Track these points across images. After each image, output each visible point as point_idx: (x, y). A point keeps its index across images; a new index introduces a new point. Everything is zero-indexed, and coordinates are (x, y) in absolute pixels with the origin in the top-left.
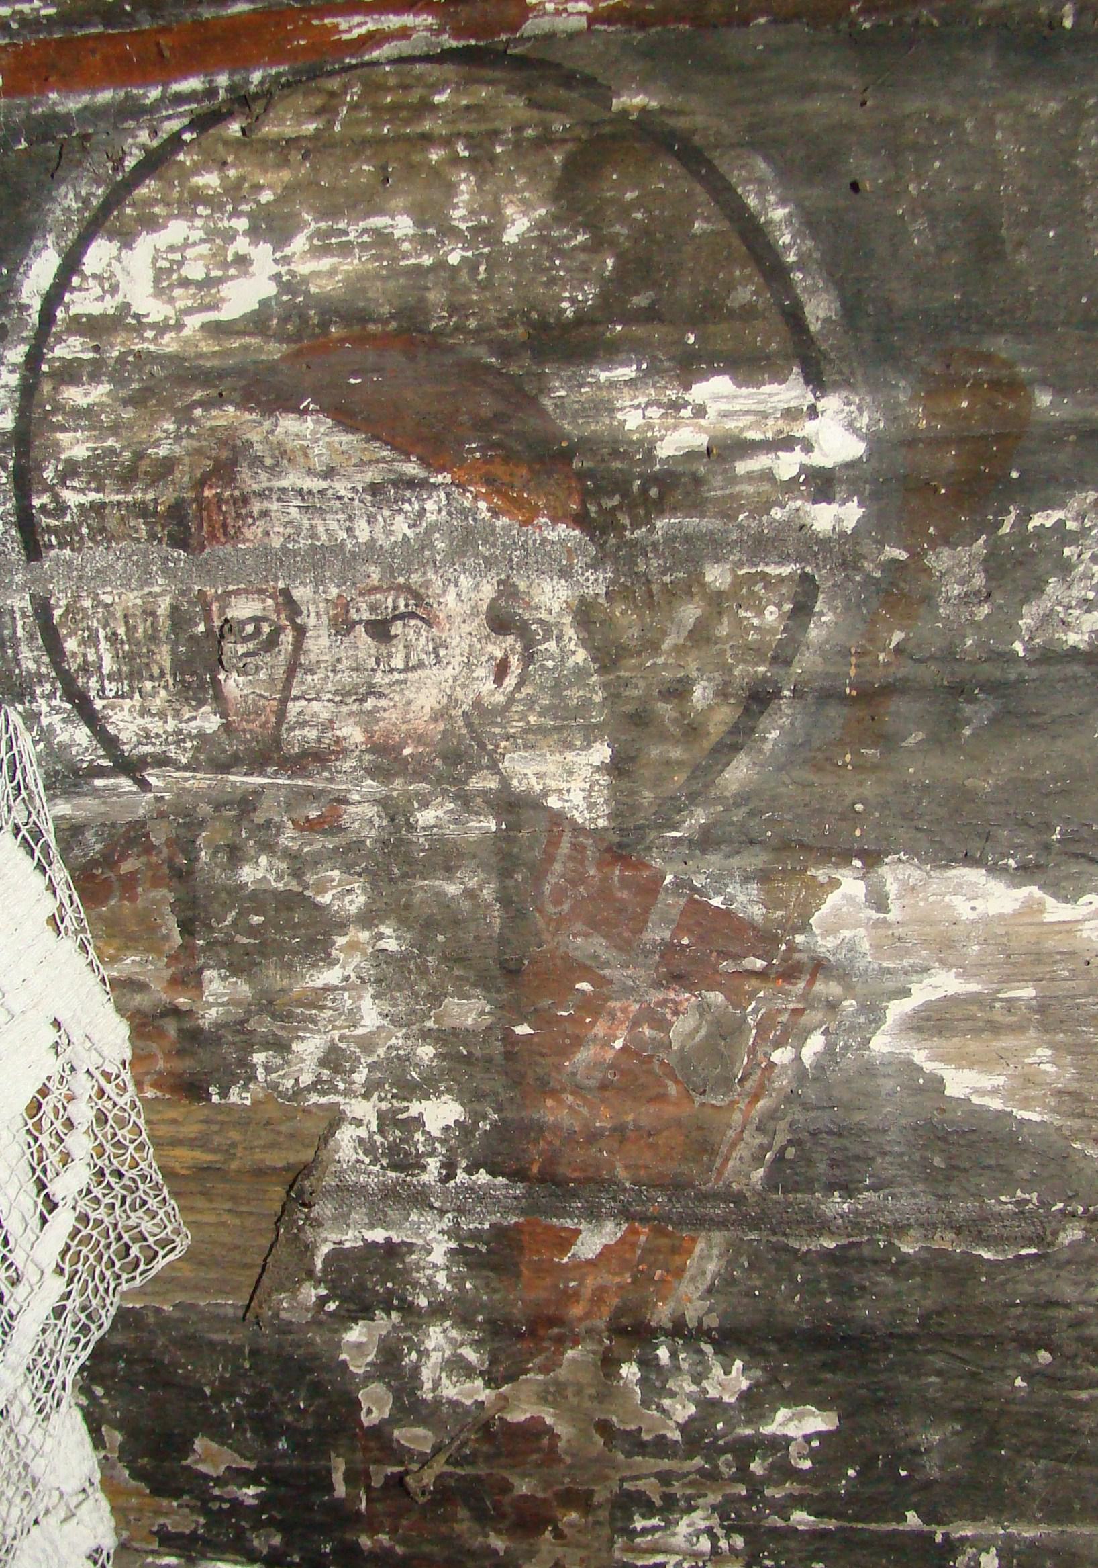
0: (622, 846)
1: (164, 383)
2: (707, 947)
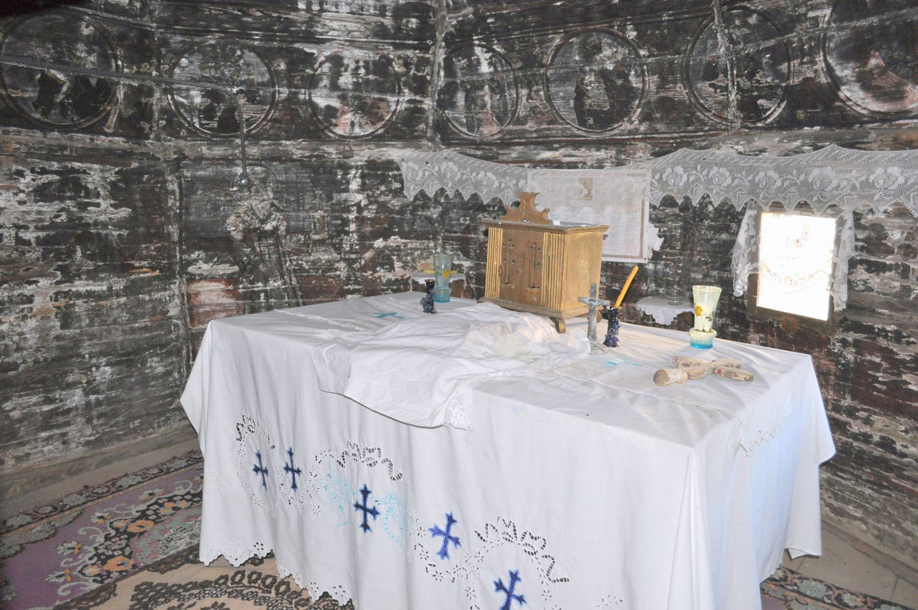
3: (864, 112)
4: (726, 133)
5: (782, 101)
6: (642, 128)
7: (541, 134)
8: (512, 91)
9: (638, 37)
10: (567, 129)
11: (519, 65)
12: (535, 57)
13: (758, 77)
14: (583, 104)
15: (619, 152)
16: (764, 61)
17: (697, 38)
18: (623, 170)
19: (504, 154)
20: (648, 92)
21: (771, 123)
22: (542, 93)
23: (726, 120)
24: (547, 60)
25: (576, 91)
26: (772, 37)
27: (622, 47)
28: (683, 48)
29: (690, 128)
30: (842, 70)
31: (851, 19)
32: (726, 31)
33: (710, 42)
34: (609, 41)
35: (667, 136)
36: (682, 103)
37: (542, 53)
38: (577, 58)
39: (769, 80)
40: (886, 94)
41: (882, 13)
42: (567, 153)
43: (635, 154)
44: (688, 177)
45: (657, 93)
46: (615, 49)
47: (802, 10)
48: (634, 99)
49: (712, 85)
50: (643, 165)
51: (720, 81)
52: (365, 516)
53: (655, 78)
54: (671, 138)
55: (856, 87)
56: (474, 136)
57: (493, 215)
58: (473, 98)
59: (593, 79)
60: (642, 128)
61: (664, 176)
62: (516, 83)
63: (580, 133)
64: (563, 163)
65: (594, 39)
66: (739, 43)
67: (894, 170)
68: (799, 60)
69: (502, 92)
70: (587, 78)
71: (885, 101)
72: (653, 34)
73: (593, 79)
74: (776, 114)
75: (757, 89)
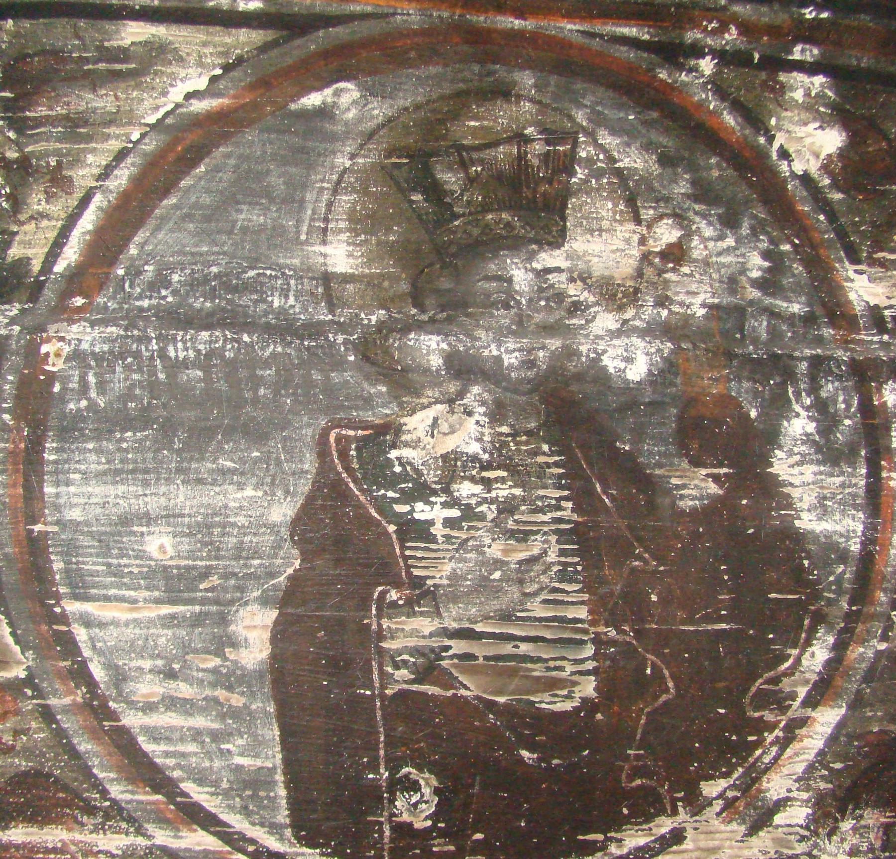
25: (303, 527)
27: (730, 222)
34: (634, 160)
38: (340, 256)
46: (667, 234)
48: (795, 625)
59: (469, 436)
65: (519, 113)
70: (417, 424)
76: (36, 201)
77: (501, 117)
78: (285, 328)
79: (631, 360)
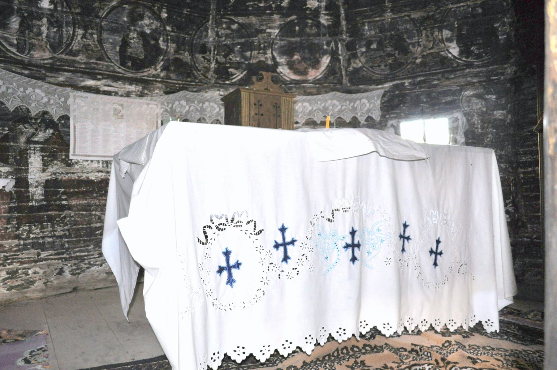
0: (487, 111)
1: (467, 97)
2: (490, 114)
3: (288, 79)
4: (206, 85)
5: (244, 70)
6: (162, 75)
7: (88, 66)
8: (69, 28)
9: (167, 17)
10: (112, 66)
11: (78, 11)
12: (94, 9)
13: (231, 57)
14: (126, 51)
15: (144, 88)
16: (236, 49)
17: (199, 29)
18: (144, 100)
19: (51, 77)
20: (169, 53)
21: (235, 82)
22: (95, 36)
23: (207, 78)
24: (102, 14)
25: (122, 40)
26: (243, 37)
27: (157, 21)
28: (190, 32)
29: (189, 79)
30: (280, 59)
31: (288, 36)
32: (216, 29)
33: (204, 33)
34: (150, 15)
35: (175, 82)
36: (186, 63)
37: (100, 8)
38: (125, 19)
39: (238, 59)
40: (299, 72)
41: (302, 36)
42: (107, 83)
43: (154, 90)
44: (190, 107)
45: (174, 54)
46: (152, 21)
47: (264, 28)
48: (160, 55)
49: (203, 57)
50: (155, 98)
51: (207, 55)
52: (404, 242)
53: (174, 45)
54: (178, 84)
55: (286, 68)
56: (24, 57)
57: (35, 127)
58: (29, 25)
59: (135, 36)
60: (162, 75)
61: (174, 106)
62: (74, 24)
63: (120, 70)
64: (100, 91)
65: (140, 10)
66: (222, 37)
67: (306, 104)
68: (257, 52)
69: (60, 27)
70: (131, 34)
71: (298, 75)
72: (176, 19)
73: (135, 36)
74: (239, 77)
75: (229, 63)
76: (101, 11)
77: (139, 10)
78: (121, 24)
79: (148, 32)
